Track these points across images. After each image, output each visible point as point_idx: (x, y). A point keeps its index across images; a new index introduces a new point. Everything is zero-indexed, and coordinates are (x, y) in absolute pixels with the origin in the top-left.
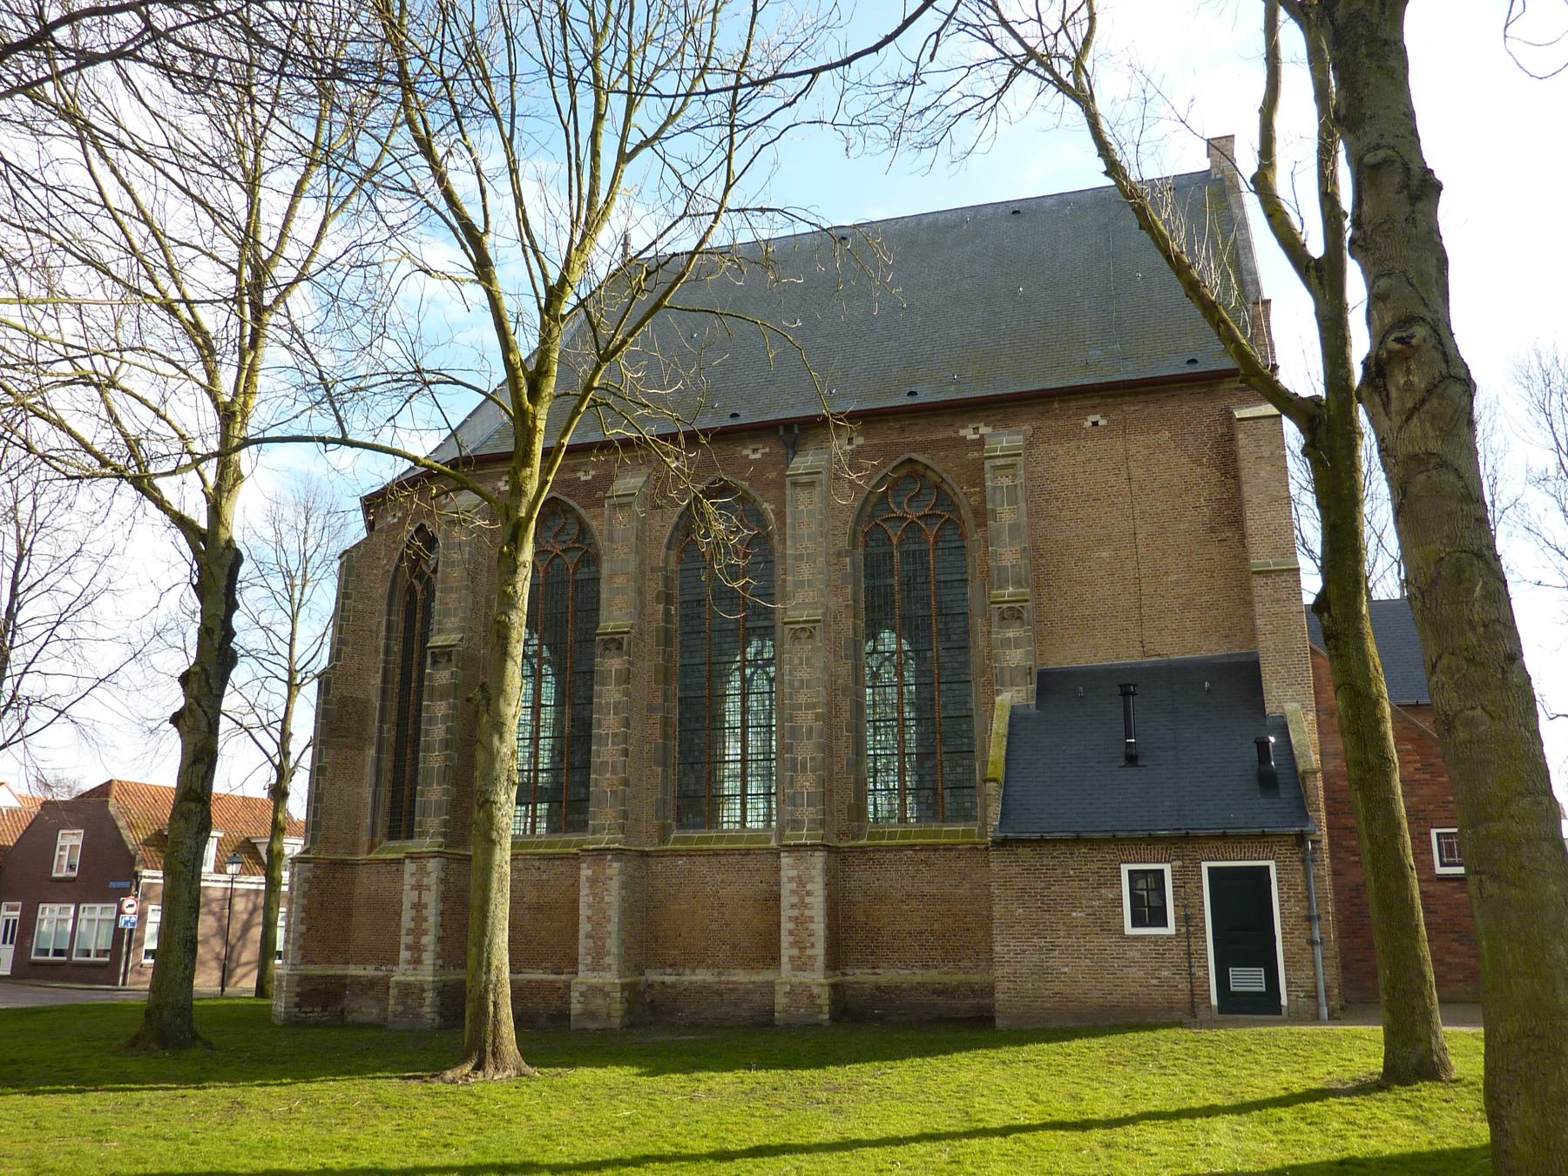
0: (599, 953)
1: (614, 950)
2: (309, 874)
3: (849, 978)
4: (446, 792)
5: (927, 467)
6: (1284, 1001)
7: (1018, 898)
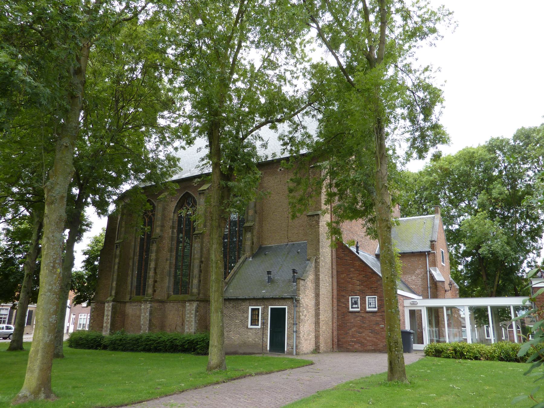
6: (286, 350)
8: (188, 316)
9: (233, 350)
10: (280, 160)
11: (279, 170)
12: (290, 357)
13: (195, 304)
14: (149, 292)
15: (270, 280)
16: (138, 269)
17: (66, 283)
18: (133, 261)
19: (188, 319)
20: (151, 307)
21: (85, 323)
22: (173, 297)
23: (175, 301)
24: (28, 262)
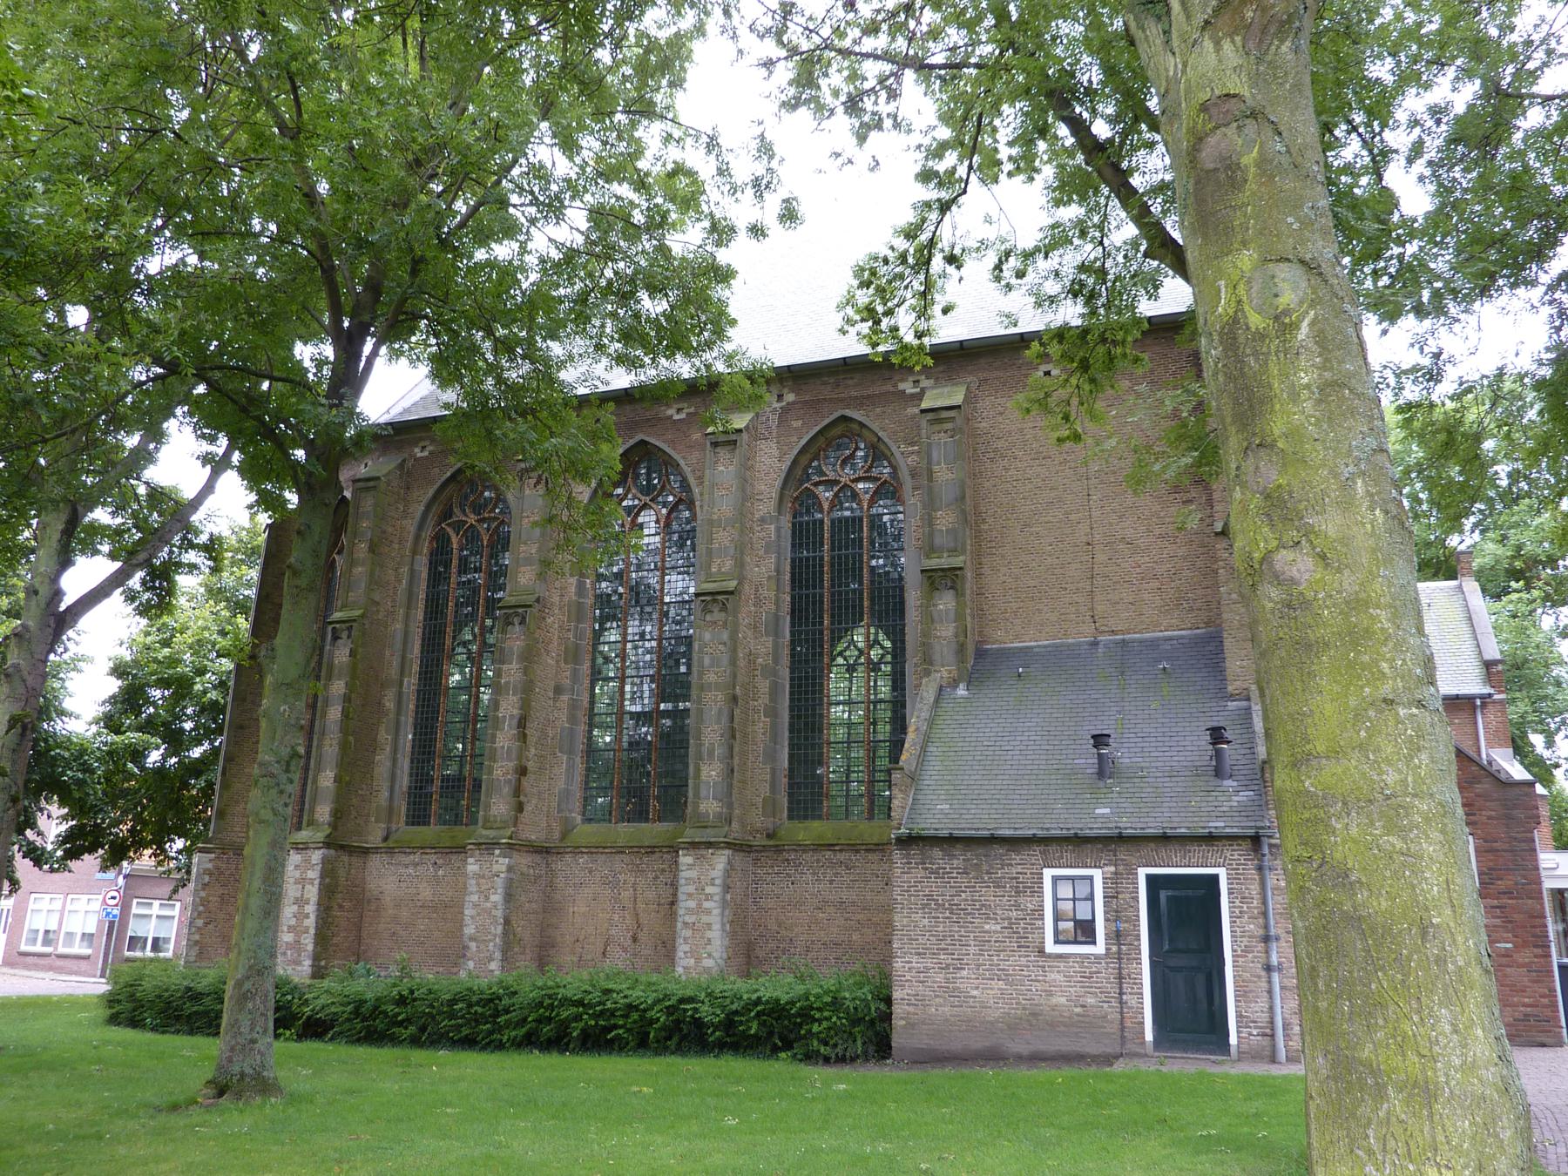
2: (210, 866)
5: (862, 425)
6: (1233, 1040)
7: (924, 906)
8: (692, 904)
9: (978, 1043)
10: (1024, 340)
12: (1261, 1069)
13: (720, 862)
14: (494, 811)
15: (1104, 769)
17: (285, 752)
18: (400, 694)
19: (688, 919)
20: (510, 869)
21: (53, 926)
22: (585, 832)
23: (594, 849)
24: (16, 667)
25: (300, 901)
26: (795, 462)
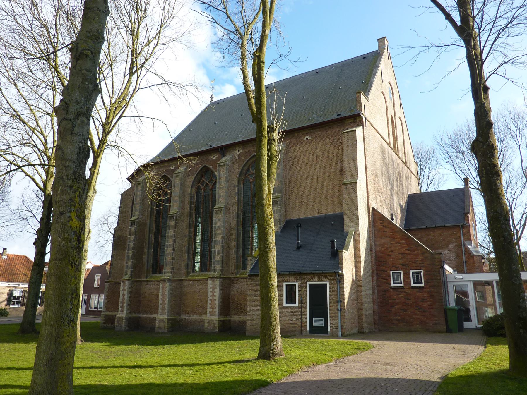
0: (163, 309)
1: (167, 309)
3: (232, 319)
4: (132, 262)
6: (329, 330)
11: (305, 139)
16: (154, 247)
25: (123, 295)
26: (242, 169)
